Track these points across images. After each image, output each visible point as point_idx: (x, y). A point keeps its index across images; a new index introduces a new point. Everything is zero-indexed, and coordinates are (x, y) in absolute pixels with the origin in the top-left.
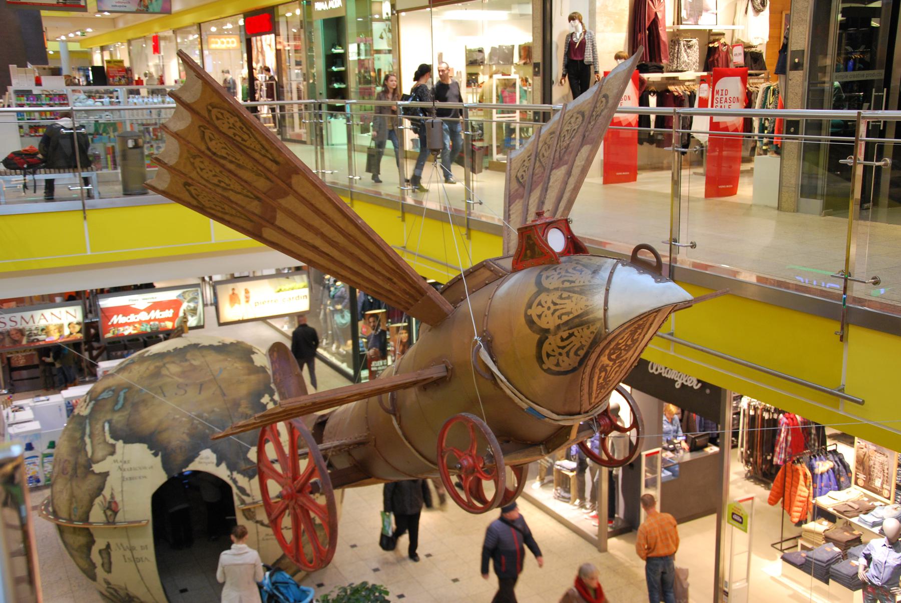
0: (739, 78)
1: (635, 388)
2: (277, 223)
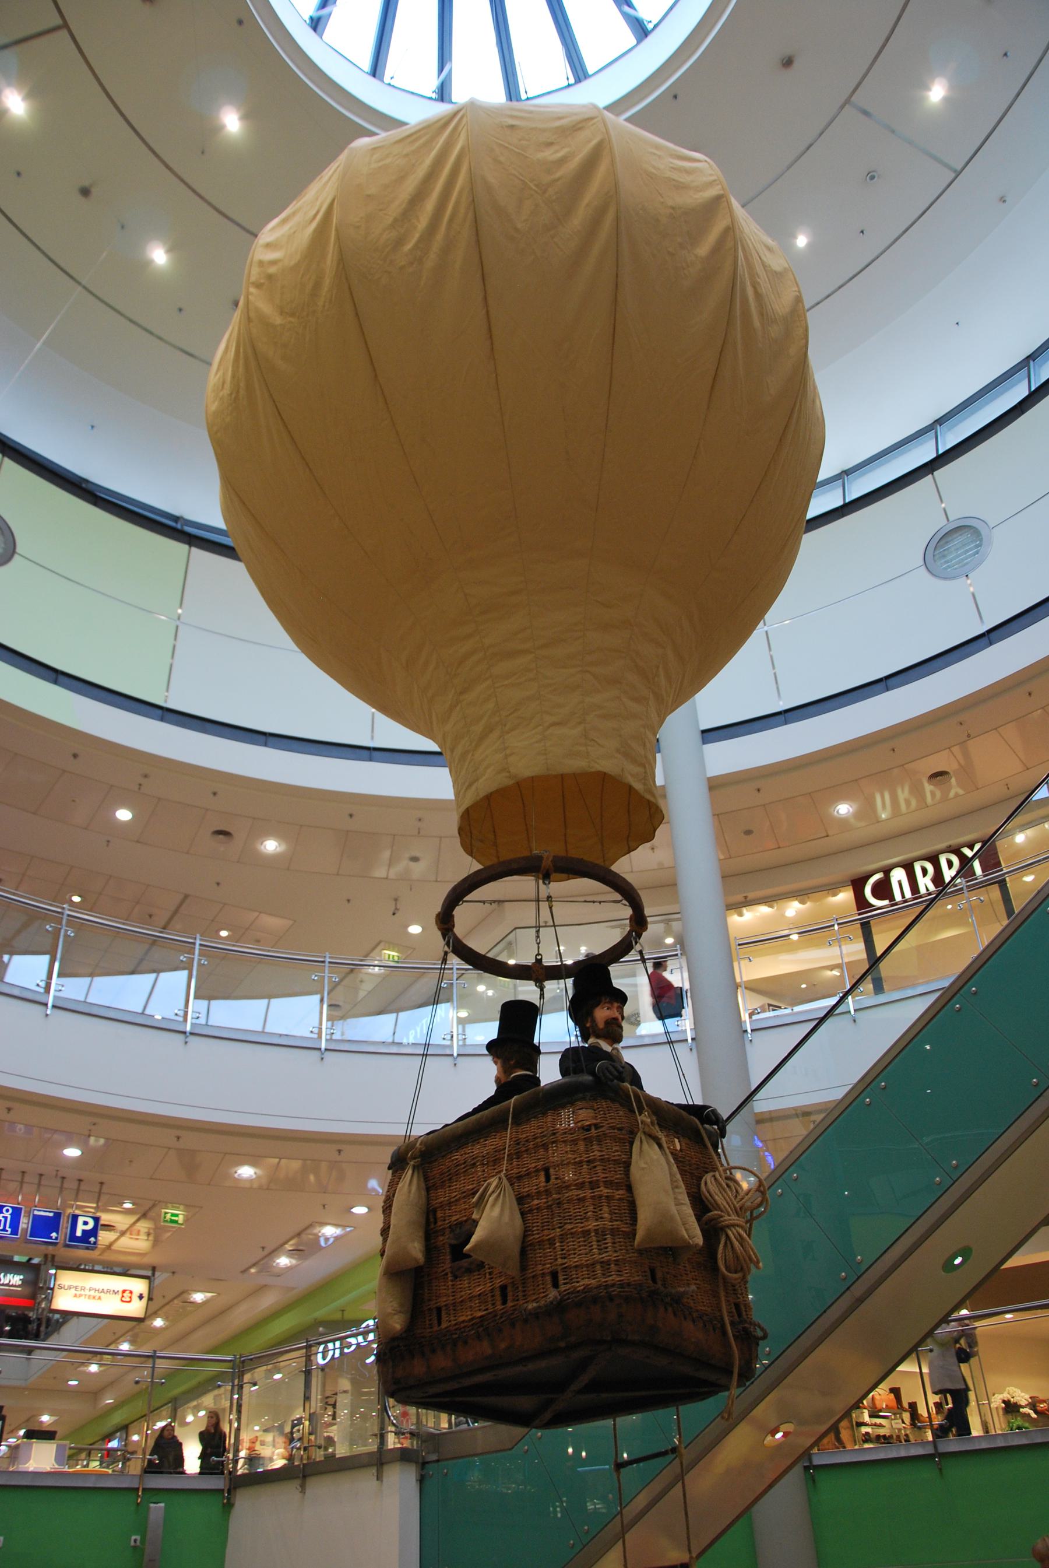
0: (447, 770)
1: (685, 1105)
2: (324, 37)
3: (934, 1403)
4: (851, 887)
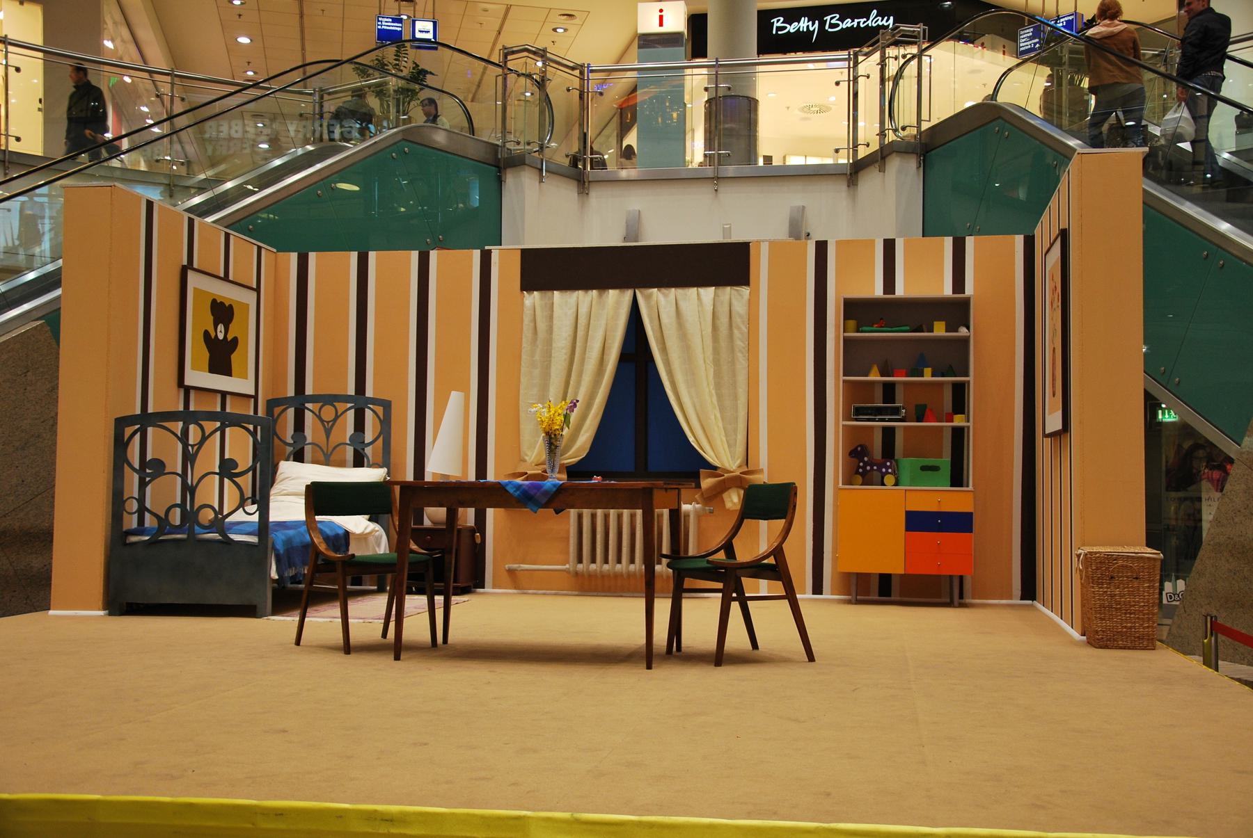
0: (382, 408)
1: (1230, 35)
3: (946, 332)
4: (670, 600)
